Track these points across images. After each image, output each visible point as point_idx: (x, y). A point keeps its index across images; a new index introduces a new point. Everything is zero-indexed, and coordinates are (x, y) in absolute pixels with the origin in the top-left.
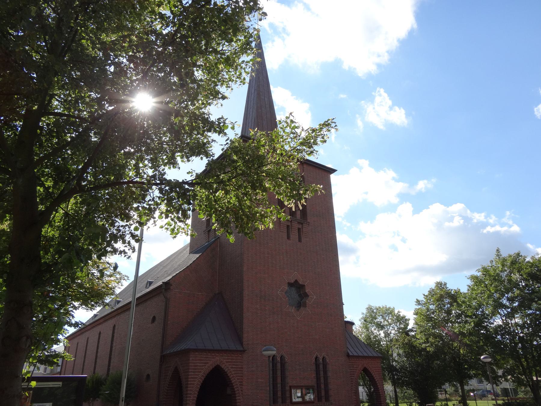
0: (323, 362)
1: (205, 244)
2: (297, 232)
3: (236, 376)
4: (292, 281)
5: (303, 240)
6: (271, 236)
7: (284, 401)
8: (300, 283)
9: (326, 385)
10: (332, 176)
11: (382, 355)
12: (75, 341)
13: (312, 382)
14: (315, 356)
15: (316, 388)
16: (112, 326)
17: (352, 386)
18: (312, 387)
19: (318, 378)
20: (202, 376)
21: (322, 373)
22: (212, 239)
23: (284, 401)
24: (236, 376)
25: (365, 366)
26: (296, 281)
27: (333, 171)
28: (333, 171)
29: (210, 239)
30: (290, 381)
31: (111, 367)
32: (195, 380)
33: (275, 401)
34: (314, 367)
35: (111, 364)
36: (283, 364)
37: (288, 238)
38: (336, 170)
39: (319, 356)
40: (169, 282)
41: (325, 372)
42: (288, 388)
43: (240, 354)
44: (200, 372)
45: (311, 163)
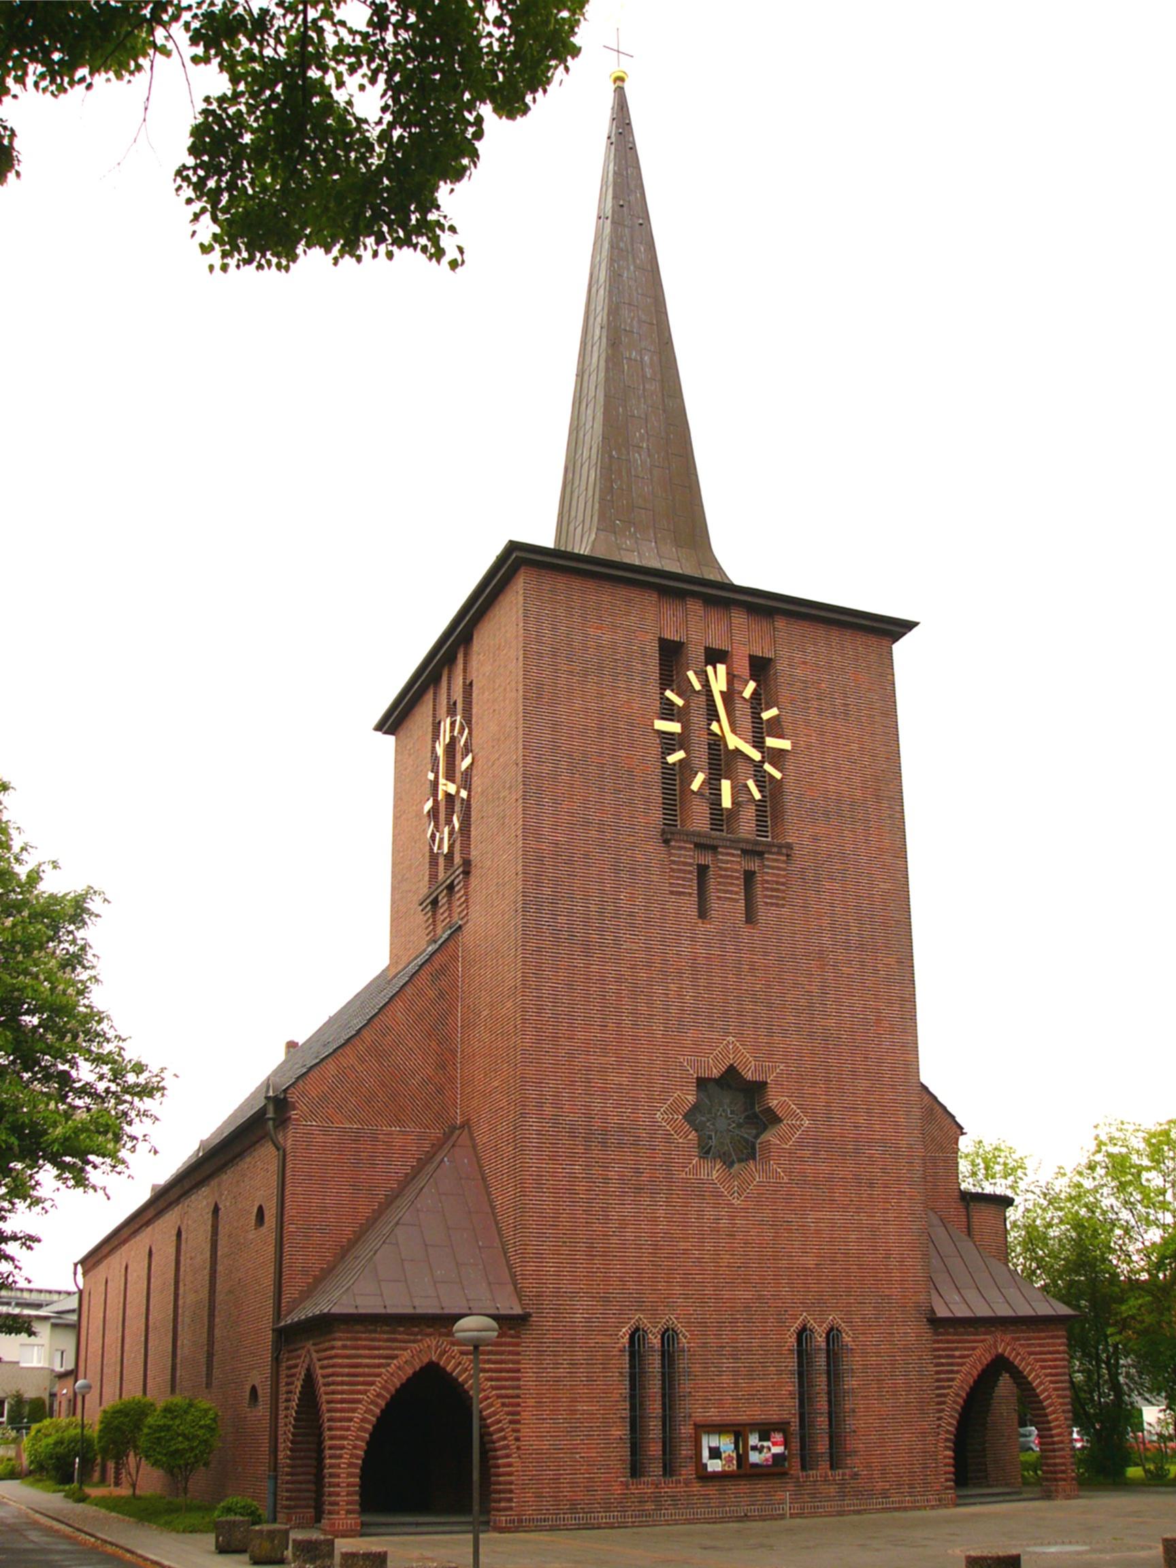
0: (828, 1344)
1: (425, 950)
2: (738, 888)
3: (499, 1397)
4: (716, 1073)
5: (765, 914)
6: (631, 914)
7: (669, 1469)
8: (749, 1076)
9: (834, 1417)
10: (901, 649)
11: (1074, 1309)
12: (102, 1271)
13: (784, 1407)
14: (797, 1325)
15: (795, 1426)
16: (174, 1232)
17: (939, 1419)
18: (782, 1427)
19: (804, 1397)
20: (378, 1395)
21: (821, 1382)
22: (444, 933)
23: (669, 1469)
24: (499, 1397)
25: (1000, 1350)
26: (731, 1069)
27: (897, 628)
28: (897, 628)
29: (439, 930)
30: (696, 1408)
31: (178, 1360)
32: (358, 1408)
33: (636, 1470)
34: (793, 1364)
35: (179, 1351)
36: (668, 1357)
37: (703, 913)
38: (916, 624)
39: (812, 1323)
40: (285, 1098)
41: (834, 1375)
42: (686, 1430)
43: (510, 1329)
44: (372, 1383)
45: (803, 610)
